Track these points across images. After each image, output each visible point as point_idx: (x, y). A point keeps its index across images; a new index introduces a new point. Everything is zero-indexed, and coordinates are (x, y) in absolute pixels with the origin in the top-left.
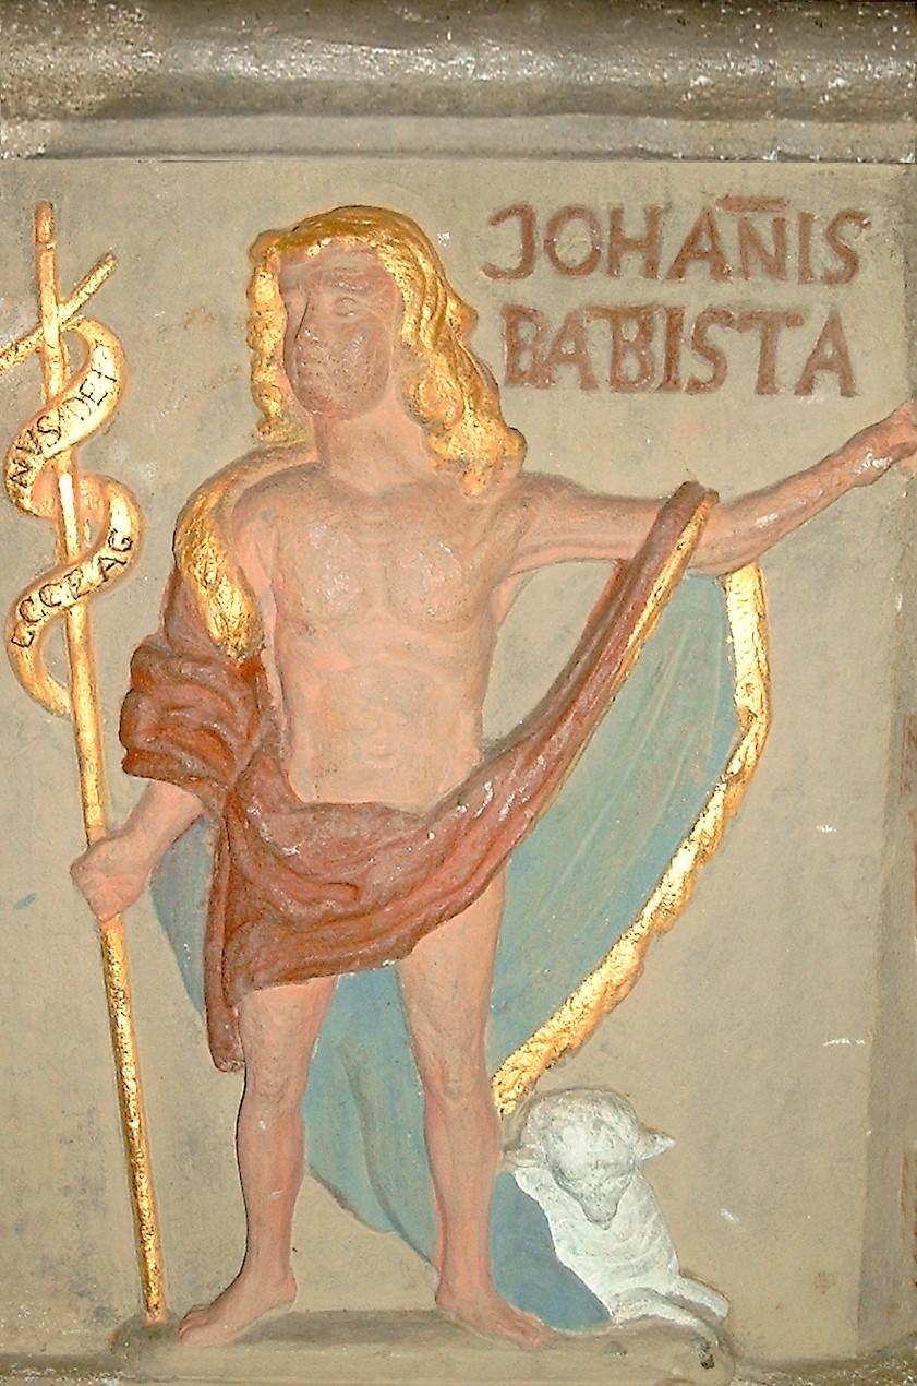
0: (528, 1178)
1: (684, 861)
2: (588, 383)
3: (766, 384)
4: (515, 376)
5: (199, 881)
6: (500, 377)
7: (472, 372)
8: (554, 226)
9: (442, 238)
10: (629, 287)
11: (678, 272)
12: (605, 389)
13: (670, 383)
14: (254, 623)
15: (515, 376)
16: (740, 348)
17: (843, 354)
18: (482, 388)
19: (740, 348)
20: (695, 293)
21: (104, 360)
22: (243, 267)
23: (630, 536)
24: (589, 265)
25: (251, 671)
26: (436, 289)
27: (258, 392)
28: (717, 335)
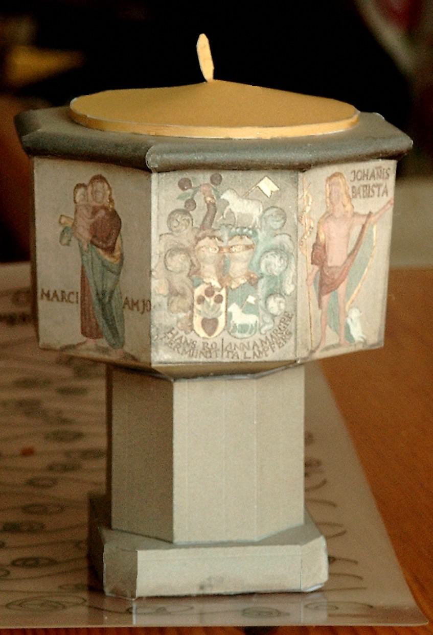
0: (349, 321)
1: (366, 270)
2: (360, 197)
3: (378, 196)
4: (353, 197)
5: (318, 279)
6: (351, 197)
7: (348, 196)
8: (358, 173)
9: (345, 176)
10: (364, 182)
11: (370, 179)
12: (362, 198)
13: (369, 196)
14: (325, 239)
15: (353, 197)
16: (376, 189)
17: (387, 190)
18: (350, 199)
19: (376, 189)
20: (372, 182)
21: (311, 200)
22: (325, 183)
23: (363, 220)
24: (361, 179)
25: (324, 247)
26: (345, 184)
27: (326, 203)
28: (374, 188)
